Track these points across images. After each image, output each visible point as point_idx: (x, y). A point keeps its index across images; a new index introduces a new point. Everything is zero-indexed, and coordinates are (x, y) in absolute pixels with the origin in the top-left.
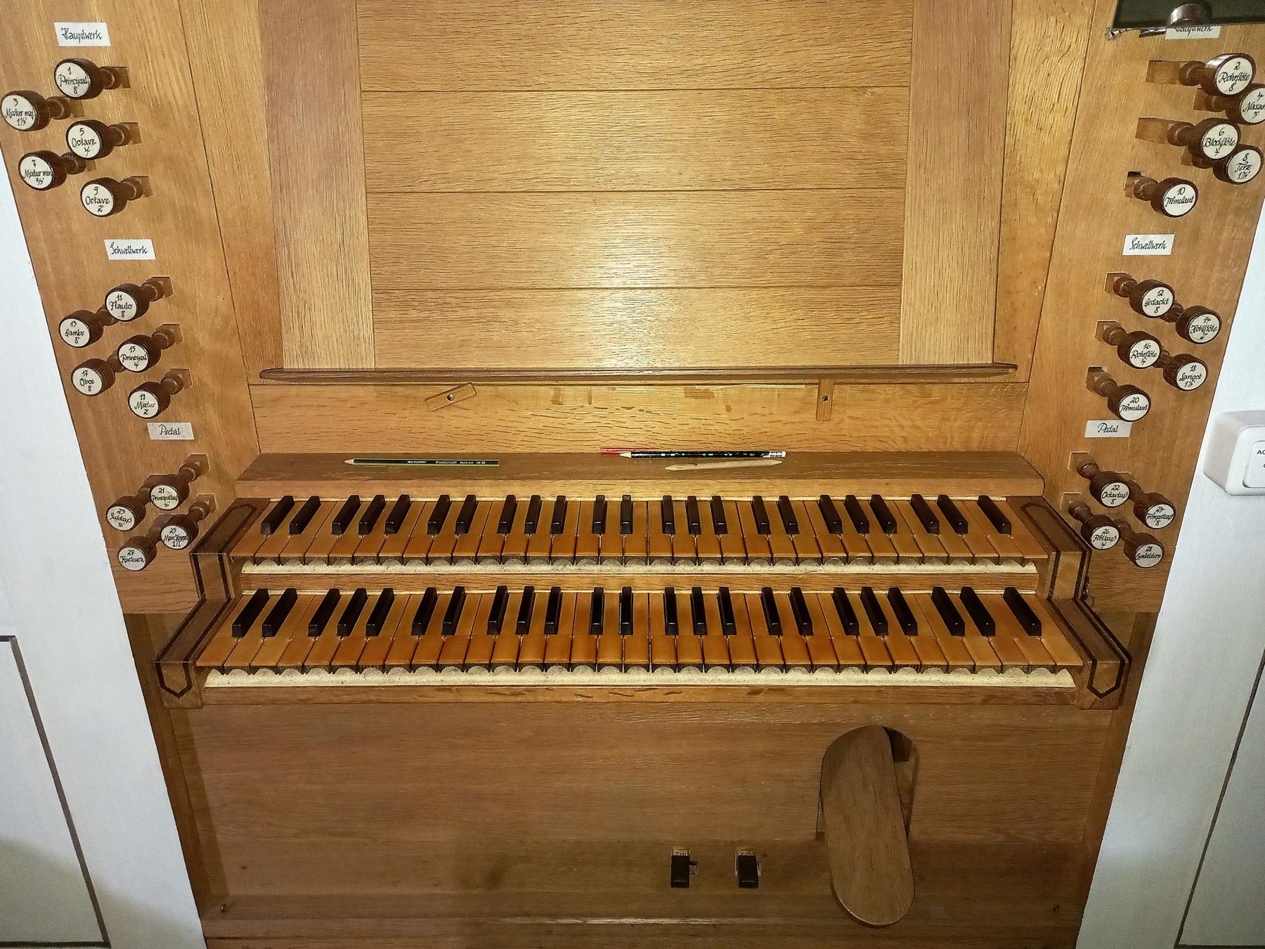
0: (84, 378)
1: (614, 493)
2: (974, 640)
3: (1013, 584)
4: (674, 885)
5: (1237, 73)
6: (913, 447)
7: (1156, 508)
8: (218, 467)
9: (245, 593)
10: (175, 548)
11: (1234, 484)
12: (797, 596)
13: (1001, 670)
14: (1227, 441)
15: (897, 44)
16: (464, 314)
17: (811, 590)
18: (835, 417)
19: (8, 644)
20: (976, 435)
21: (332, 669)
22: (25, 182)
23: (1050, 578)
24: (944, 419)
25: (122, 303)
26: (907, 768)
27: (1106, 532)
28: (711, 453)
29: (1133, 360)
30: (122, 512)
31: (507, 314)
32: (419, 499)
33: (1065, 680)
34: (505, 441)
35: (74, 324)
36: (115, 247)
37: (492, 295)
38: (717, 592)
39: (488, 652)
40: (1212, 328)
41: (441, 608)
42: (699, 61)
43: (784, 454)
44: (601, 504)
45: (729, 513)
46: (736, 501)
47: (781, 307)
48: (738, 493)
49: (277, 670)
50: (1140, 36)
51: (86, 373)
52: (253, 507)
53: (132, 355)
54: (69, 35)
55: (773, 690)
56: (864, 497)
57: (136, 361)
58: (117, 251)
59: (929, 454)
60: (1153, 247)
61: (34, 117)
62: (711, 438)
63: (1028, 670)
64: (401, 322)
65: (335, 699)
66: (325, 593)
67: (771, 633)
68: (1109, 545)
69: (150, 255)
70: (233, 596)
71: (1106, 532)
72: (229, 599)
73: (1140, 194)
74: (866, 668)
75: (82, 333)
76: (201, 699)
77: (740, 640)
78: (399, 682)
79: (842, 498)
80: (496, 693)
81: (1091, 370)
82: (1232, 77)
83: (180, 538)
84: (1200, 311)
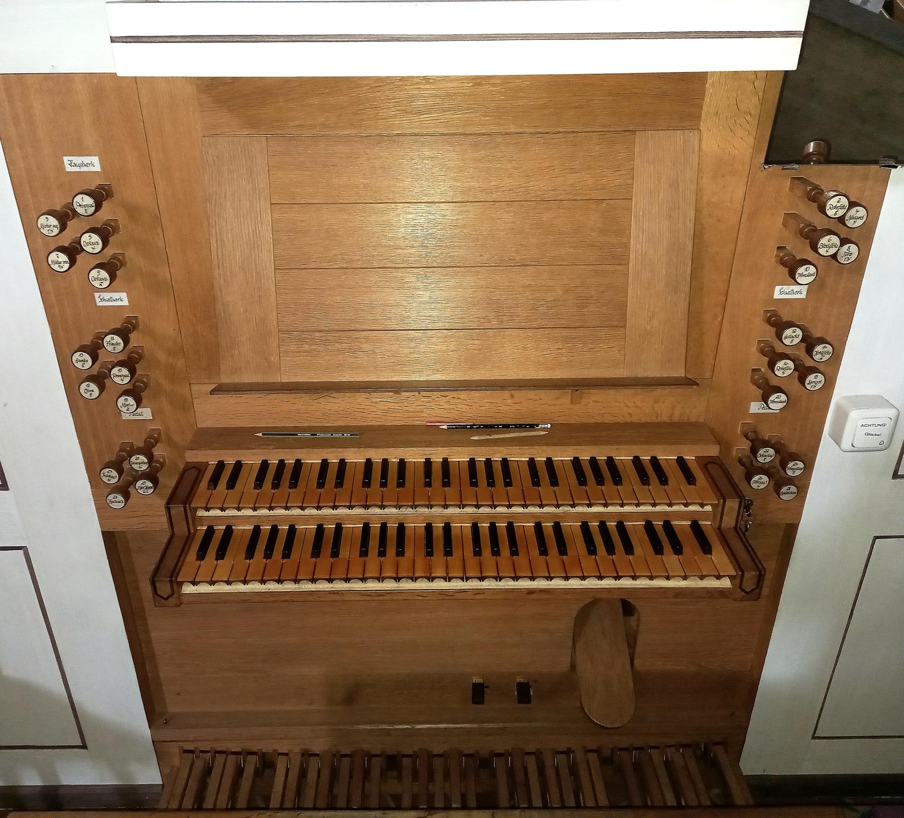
1: (437, 455)
2: (670, 559)
3: (696, 518)
4: (474, 702)
5: (839, 205)
6: (634, 419)
7: (793, 463)
8: (169, 438)
9: (199, 528)
11: (846, 443)
12: (557, 527)
13: (685, 578)
14: (842, 417)
15: (623, 172)
16: (340, 347)
17: (567, 522)
18: (584, 401)
19: (21, 553)
20: (677, 412)
21: (263, 582)
22: (52, 268)
23: (719, 515)
24: (656, 402)
26: (633, 621)
27: (761, 478)
28: (500, 425)
29: (776, 372)
30: (110, 472)
31: (366, 347)
32: (308, 461)
33: (726, 583)
34: (361, 418)
37: (357, 334)
38: (506, 524)
39: (361, 570)
40: (828, 353)
41: (329, 537)
42: (493, 183)
43: (549, 426)
44: (428, 463)
45: (513, 468)
46: (517, 461)
47: (548, 341)
48: (519, 456)
49: (229, 583)
50: (782, 169)
52: (199, 469)
53: (120, 374)
54: (73, 164)
55: (543, 591)
56: (602, 458)
57: (122, 378)
58: (103, 300)
59: (645, 425)
62: (500, 415)
63: (702, 578)
64: (298, 352)
65: (265, 600)
66: (252, 527)
67: (541, 554)
68: (762, 486)
69: (125, 302)
70: (192, 531)
71: (761, 478)
72: (189, 533)
73: (783, 263)
74: (600, 578)
76: (180, 600)
77: (522, 560)
78: (305, 589)
79: (588, 458)
80: (366, 595)
81: (753, 370)
82: (836, 207)
83: (147, 488)
84: (822, 341)
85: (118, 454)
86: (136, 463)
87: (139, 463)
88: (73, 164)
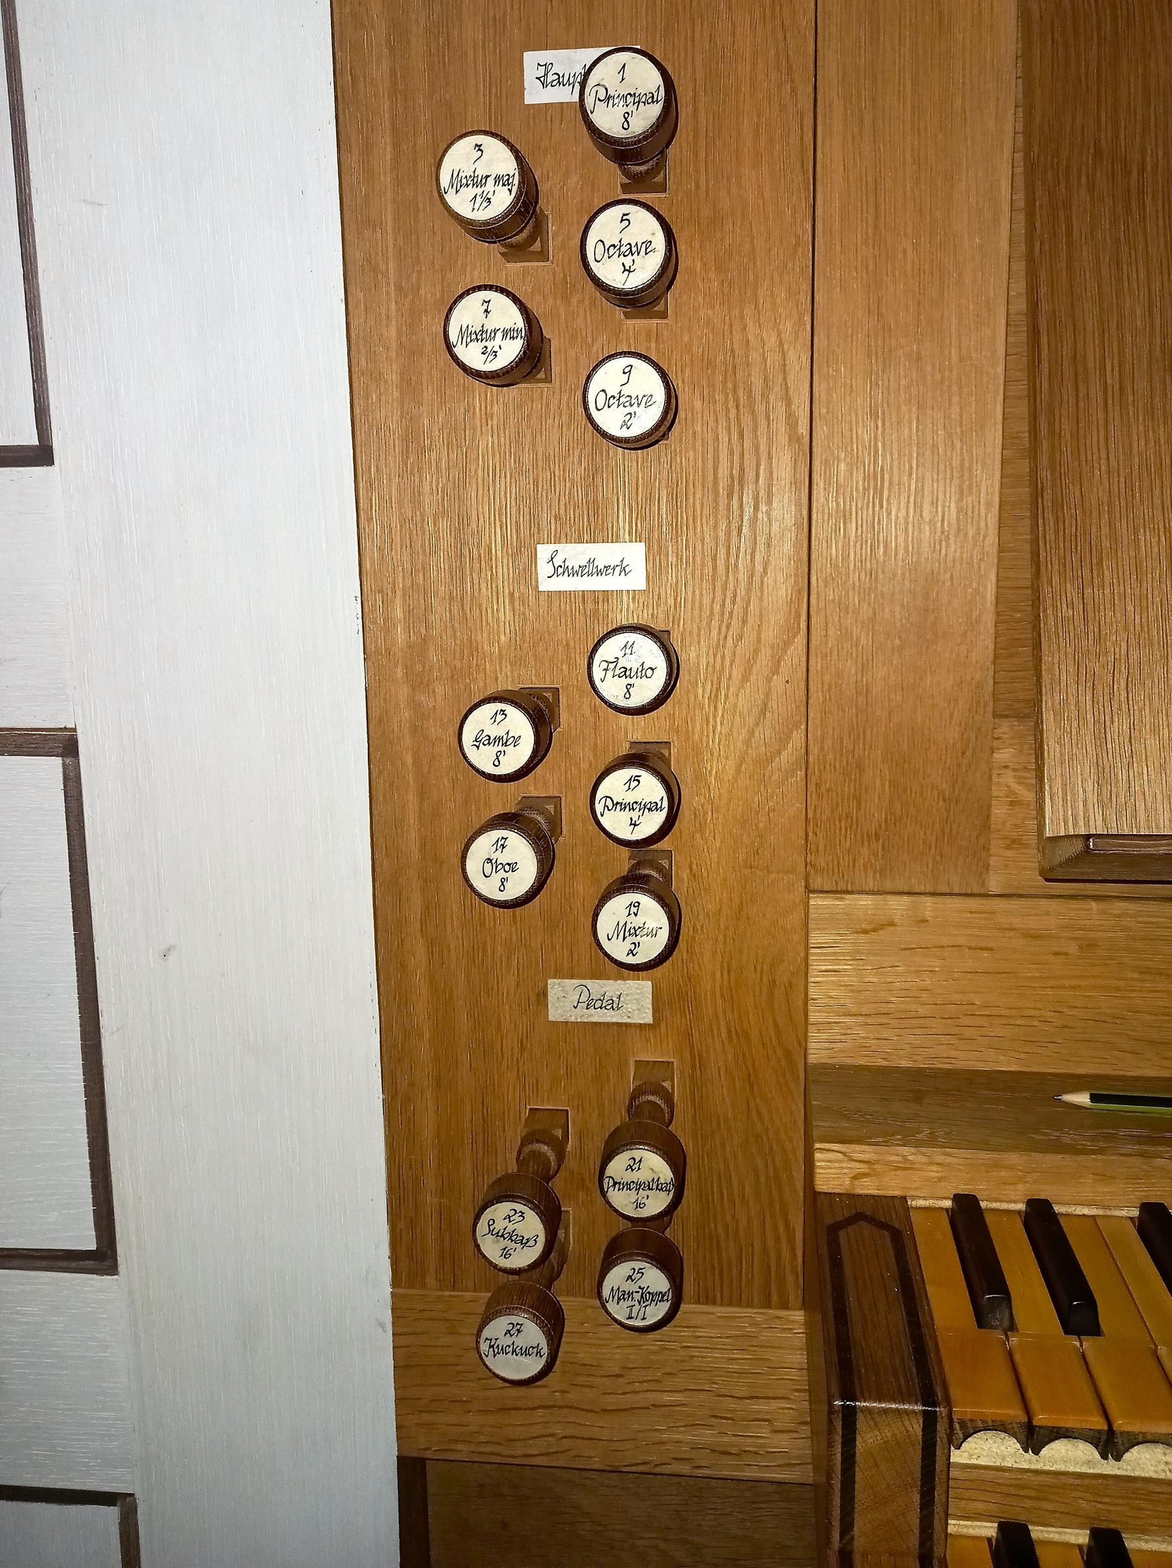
0: (494, 857)
10: (630, 1322)
25: (631, 662)
30: (517, 1218)
35: (500, 717)
36: (558, 561)
51: (501, 845)
53: (630, 798)
57: (635, 815)
58: (563, 570)
60: (599, 573)
61: (515, 189)
75: (516, 741)
85: (527, 1149)
86: (627, 1186)
87: (639, 1186)
88: (550, 78)
